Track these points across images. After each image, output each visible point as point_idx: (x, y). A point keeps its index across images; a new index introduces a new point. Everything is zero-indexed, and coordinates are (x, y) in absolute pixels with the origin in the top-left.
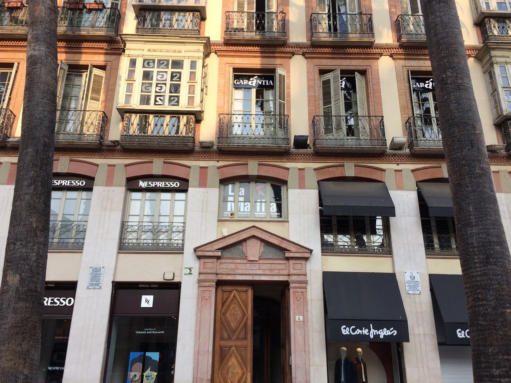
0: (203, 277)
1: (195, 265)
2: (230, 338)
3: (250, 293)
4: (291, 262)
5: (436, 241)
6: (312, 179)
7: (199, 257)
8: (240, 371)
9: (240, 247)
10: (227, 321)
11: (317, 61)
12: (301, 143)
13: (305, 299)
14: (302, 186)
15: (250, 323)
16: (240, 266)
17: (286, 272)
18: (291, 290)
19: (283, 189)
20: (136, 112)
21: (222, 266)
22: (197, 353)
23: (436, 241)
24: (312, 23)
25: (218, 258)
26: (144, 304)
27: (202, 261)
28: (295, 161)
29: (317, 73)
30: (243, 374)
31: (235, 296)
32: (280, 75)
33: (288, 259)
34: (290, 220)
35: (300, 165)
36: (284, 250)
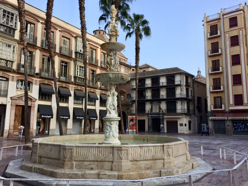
1: (10, 101)
3: (21, 107)
4: (32, 102)
6: (38, 83)
7: (12, 99)
11: (42, 52)
13: (34, 109)
14: (36, 84)
15: (21, 114)
17: (31, 104)
18: (32, 108)
19: (31, 84)
20: (78, 77)
21: (17, 101)
24: (42, 42)
25: (16, 100)
32: (34, 55)
33: (32, 101)
34: (33, 92)
36: (31, 99)
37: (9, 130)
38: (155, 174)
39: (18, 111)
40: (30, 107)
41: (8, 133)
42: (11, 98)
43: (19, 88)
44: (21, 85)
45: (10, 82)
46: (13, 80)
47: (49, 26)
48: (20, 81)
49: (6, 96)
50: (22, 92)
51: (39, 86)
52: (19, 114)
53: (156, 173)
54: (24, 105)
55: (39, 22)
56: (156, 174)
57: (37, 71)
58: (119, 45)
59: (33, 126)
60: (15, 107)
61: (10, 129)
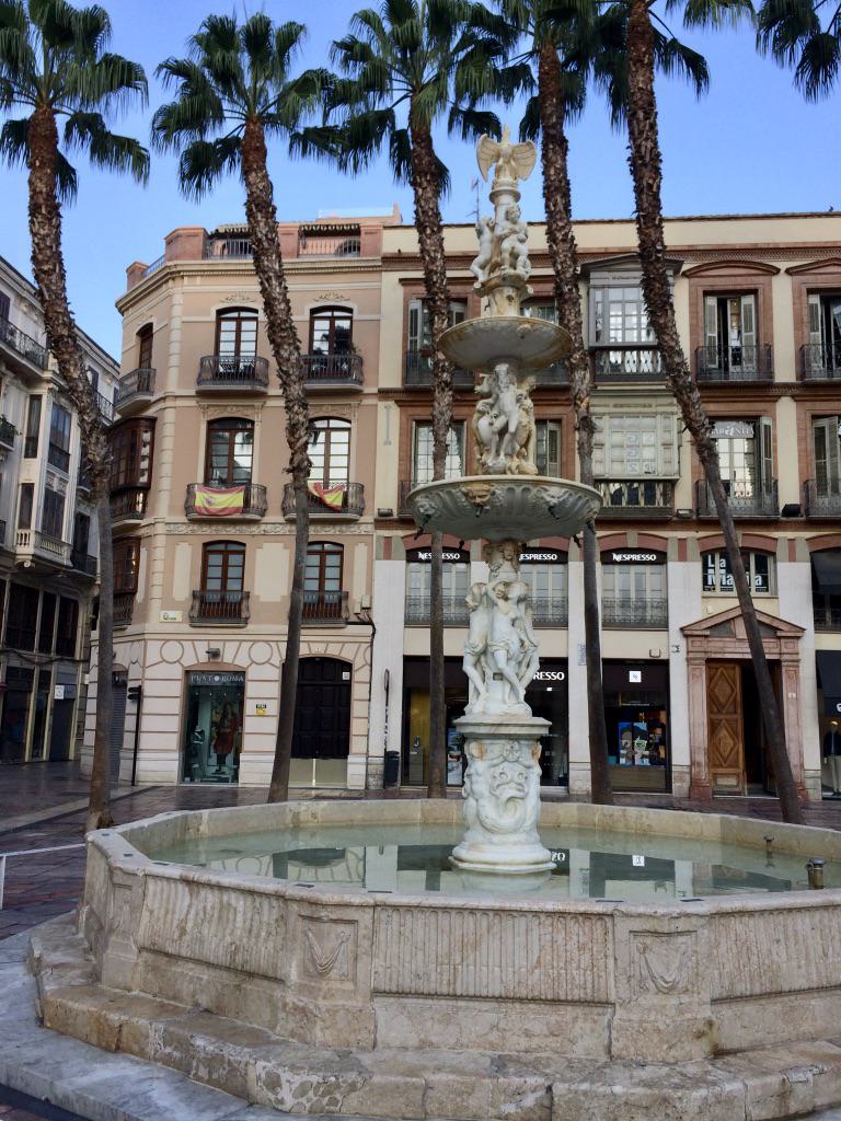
0: (691, 655)
1: (682, 643)
2: (719, 712)
3: (738, 670)
5: (828, 615)
6: (803, 551)
7: (686, 636)
8: (732, 742)
9: (728, 625)
10: (716, 696)
12: (791, 511)
13: (797, 678)
14: (792, 558)
15: (739, 698)
16: (728, 645)
17: (777, 651)
18: (784, 670)
19: (770, 561)
21: (710, 644)
22: (691, 727)
23: (828, 615)
24: (802, 357)
25: (706, 636)
26: (632, 680)
27: (690, 639)
28: (785, 529)
29: (809, 419)
30: (735, 744)
31: (722, 673)
32: (766, 426)
33: (779, 638)
35: (790, 535)
37: (690, 766)
38: (168, 1050)
39: (726, 684)
40: (775, 665)
41: (688, 777)
42: (682, 629)
43: (718, 587)
44: (724, 571)
45: (673, 566)
46: (683, 557)
47: (657, 298)
48: (717, 557)
49: (662, 625)
50: (728, 604)
51: (809, 564)
52: (731, 700)
53: (176, 1048)
54: (750, 657)
55: (774, 274)
56: (177, 1054)
57: (790, 494)
58: (481, 330)
59: (801, 755)
60: (704, 668)
61: (693, 763)
